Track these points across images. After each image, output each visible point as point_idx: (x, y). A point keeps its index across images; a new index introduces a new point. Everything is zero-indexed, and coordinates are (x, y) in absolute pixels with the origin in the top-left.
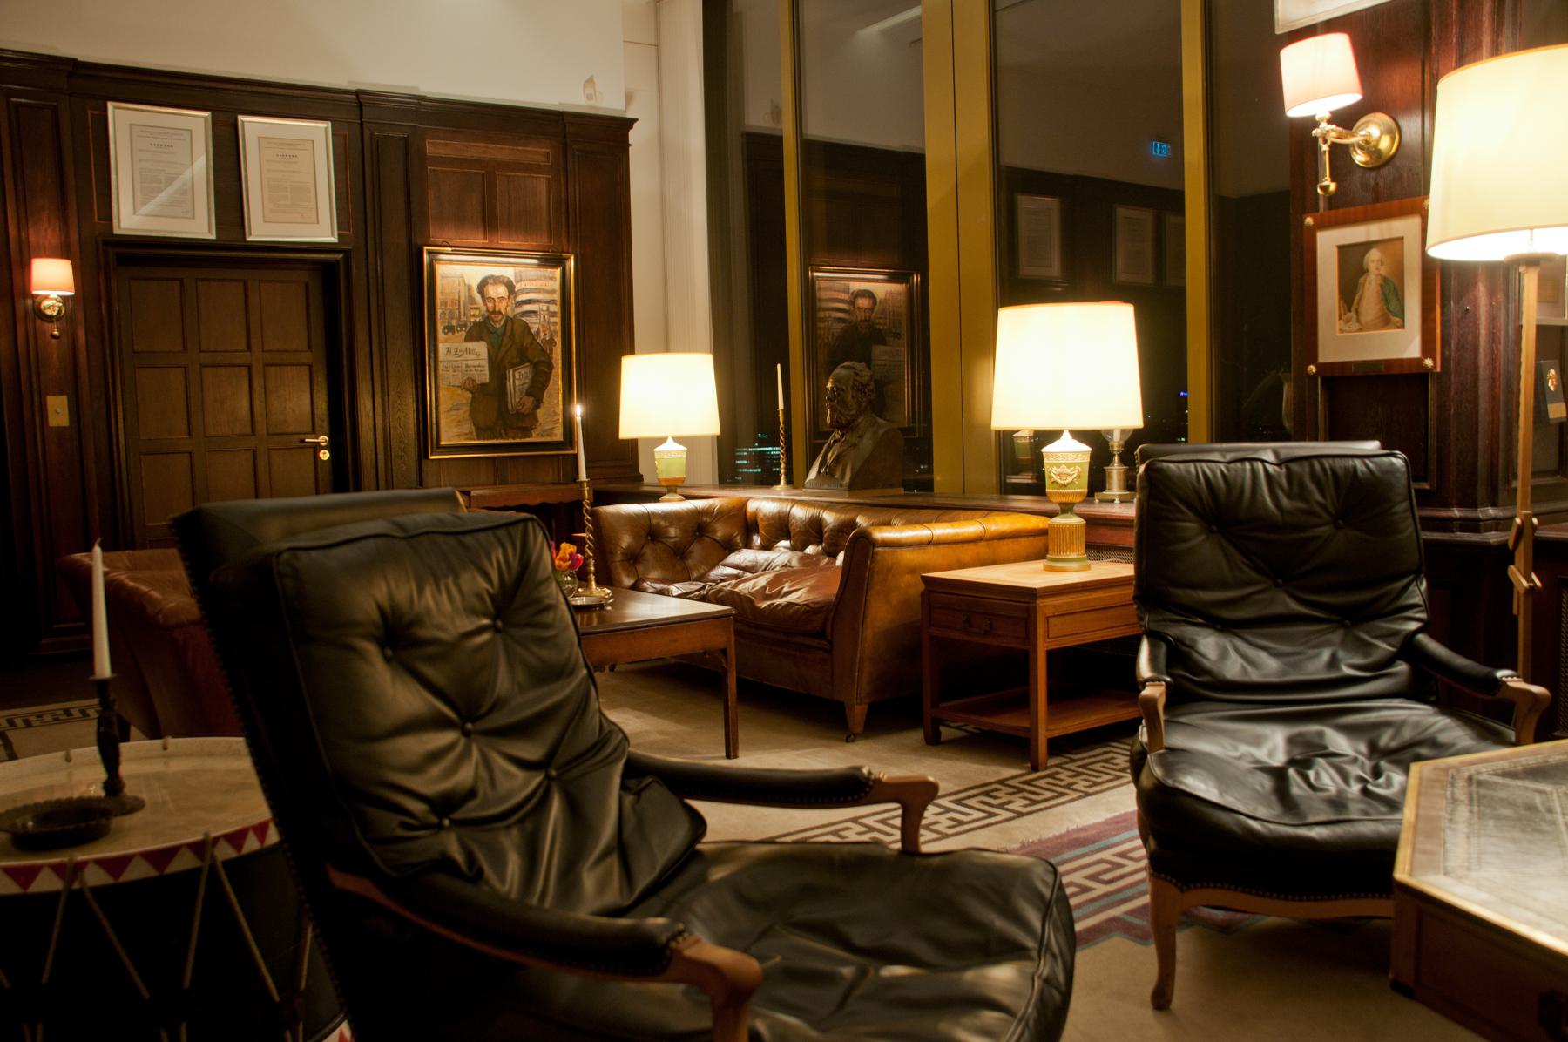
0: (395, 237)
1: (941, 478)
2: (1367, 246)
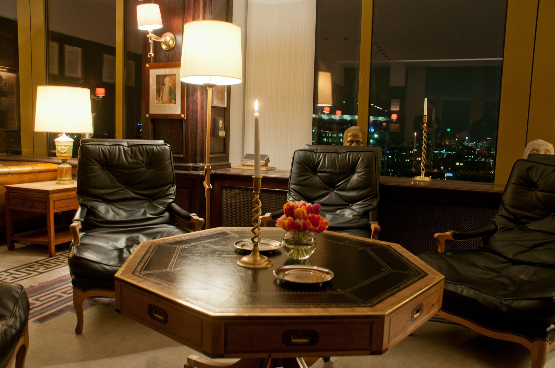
1: (25, 150)
2: (165, 76)
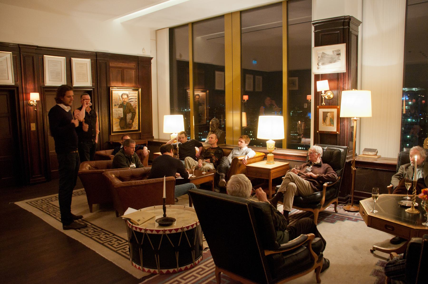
0: (104, 85)
2: (328, 112)
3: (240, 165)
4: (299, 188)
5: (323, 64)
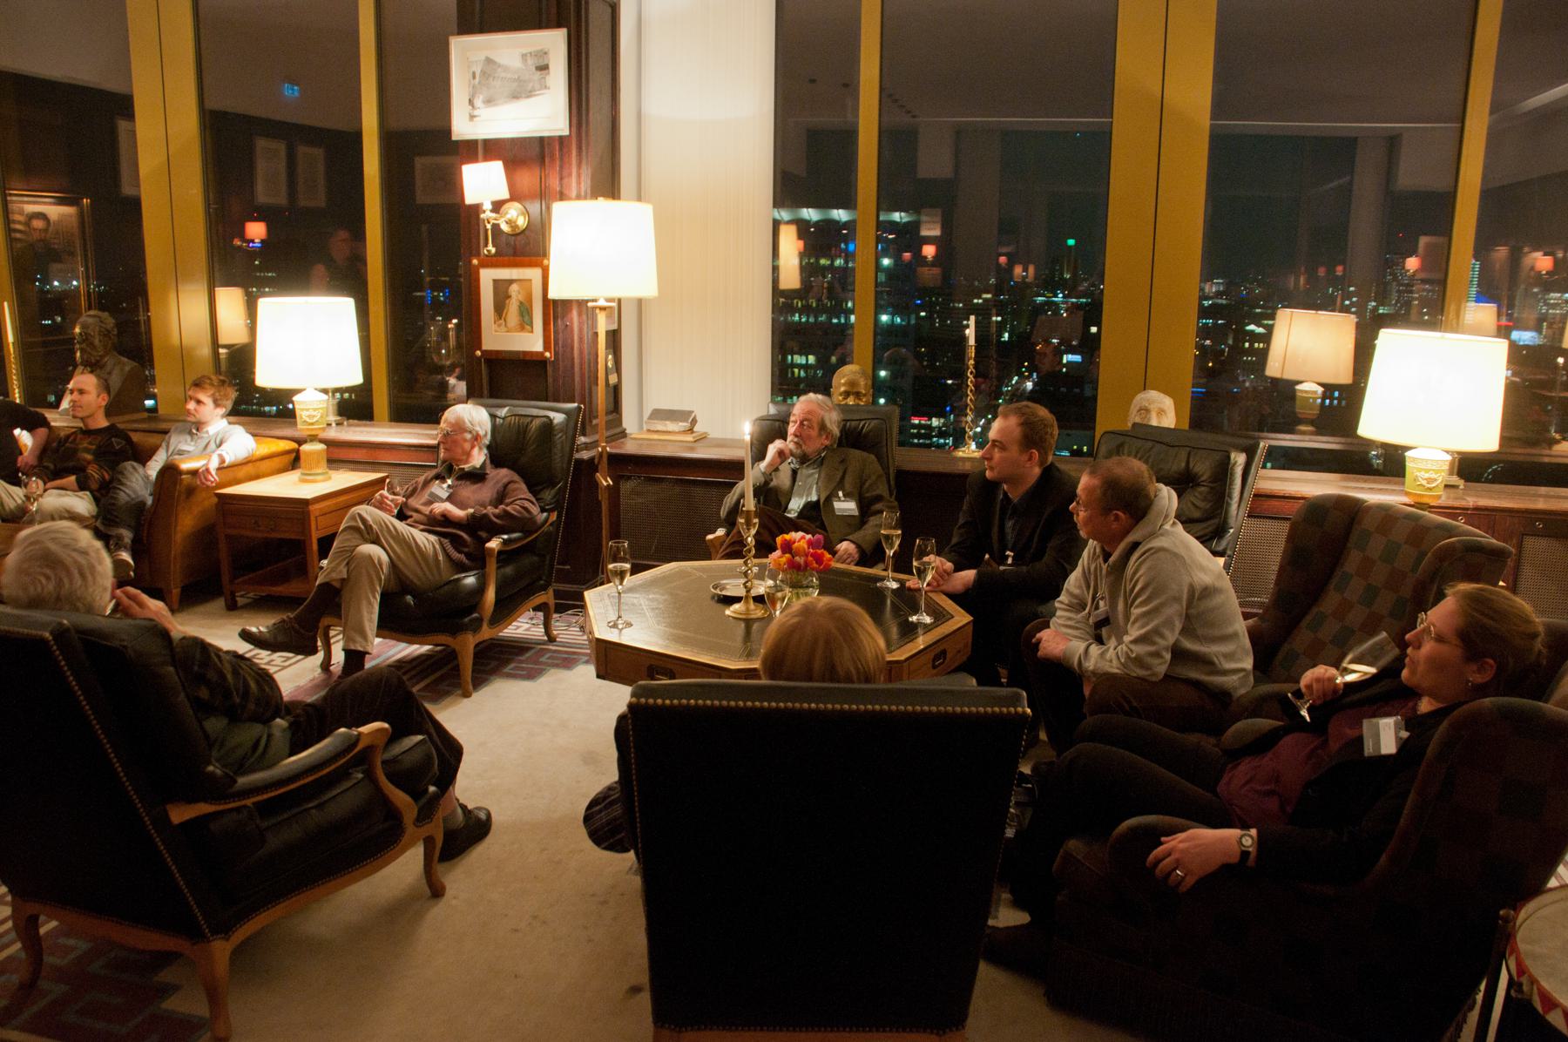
2: (511, 282)
3: (191, 491)
4: (401, 566)
5: (489, 101)
